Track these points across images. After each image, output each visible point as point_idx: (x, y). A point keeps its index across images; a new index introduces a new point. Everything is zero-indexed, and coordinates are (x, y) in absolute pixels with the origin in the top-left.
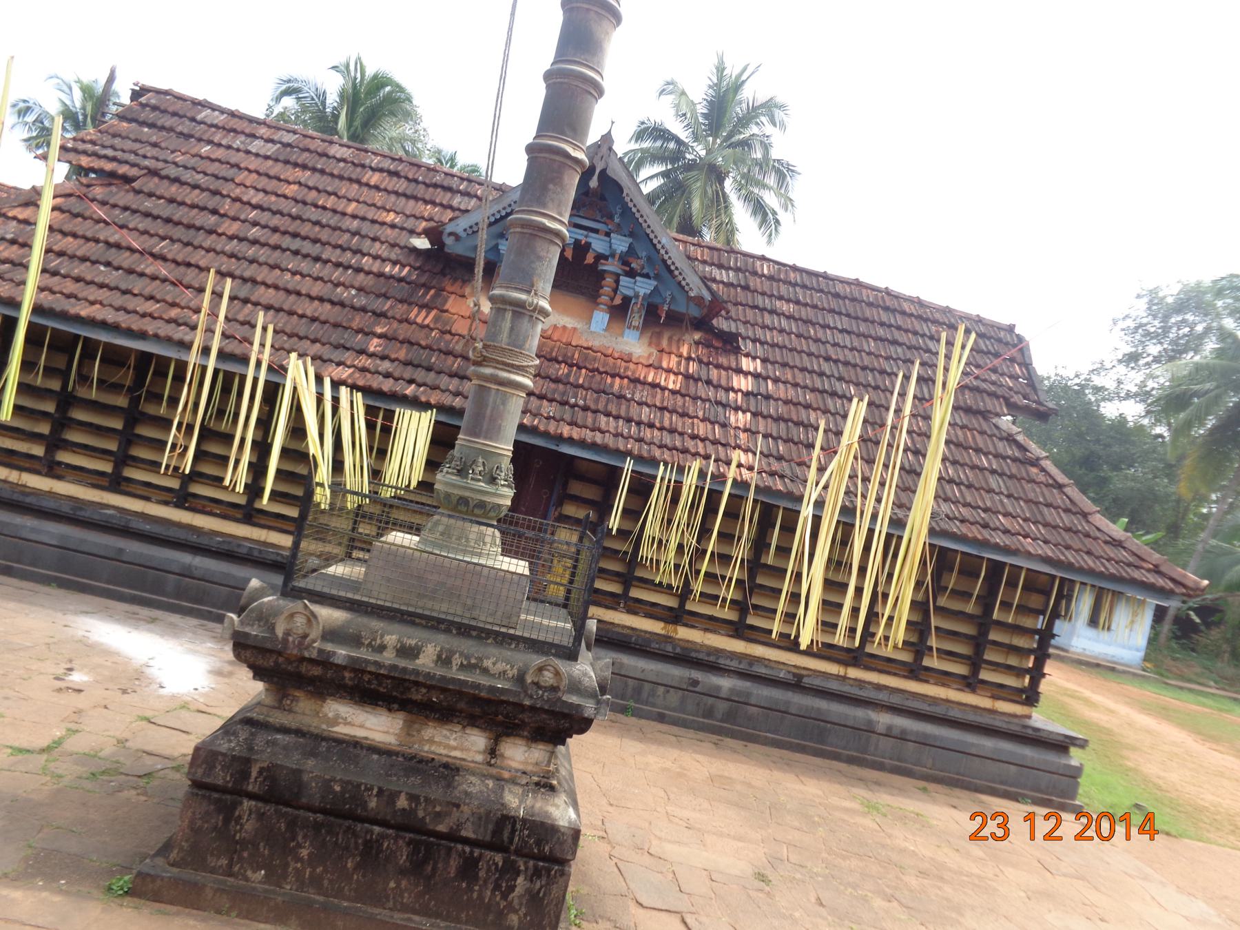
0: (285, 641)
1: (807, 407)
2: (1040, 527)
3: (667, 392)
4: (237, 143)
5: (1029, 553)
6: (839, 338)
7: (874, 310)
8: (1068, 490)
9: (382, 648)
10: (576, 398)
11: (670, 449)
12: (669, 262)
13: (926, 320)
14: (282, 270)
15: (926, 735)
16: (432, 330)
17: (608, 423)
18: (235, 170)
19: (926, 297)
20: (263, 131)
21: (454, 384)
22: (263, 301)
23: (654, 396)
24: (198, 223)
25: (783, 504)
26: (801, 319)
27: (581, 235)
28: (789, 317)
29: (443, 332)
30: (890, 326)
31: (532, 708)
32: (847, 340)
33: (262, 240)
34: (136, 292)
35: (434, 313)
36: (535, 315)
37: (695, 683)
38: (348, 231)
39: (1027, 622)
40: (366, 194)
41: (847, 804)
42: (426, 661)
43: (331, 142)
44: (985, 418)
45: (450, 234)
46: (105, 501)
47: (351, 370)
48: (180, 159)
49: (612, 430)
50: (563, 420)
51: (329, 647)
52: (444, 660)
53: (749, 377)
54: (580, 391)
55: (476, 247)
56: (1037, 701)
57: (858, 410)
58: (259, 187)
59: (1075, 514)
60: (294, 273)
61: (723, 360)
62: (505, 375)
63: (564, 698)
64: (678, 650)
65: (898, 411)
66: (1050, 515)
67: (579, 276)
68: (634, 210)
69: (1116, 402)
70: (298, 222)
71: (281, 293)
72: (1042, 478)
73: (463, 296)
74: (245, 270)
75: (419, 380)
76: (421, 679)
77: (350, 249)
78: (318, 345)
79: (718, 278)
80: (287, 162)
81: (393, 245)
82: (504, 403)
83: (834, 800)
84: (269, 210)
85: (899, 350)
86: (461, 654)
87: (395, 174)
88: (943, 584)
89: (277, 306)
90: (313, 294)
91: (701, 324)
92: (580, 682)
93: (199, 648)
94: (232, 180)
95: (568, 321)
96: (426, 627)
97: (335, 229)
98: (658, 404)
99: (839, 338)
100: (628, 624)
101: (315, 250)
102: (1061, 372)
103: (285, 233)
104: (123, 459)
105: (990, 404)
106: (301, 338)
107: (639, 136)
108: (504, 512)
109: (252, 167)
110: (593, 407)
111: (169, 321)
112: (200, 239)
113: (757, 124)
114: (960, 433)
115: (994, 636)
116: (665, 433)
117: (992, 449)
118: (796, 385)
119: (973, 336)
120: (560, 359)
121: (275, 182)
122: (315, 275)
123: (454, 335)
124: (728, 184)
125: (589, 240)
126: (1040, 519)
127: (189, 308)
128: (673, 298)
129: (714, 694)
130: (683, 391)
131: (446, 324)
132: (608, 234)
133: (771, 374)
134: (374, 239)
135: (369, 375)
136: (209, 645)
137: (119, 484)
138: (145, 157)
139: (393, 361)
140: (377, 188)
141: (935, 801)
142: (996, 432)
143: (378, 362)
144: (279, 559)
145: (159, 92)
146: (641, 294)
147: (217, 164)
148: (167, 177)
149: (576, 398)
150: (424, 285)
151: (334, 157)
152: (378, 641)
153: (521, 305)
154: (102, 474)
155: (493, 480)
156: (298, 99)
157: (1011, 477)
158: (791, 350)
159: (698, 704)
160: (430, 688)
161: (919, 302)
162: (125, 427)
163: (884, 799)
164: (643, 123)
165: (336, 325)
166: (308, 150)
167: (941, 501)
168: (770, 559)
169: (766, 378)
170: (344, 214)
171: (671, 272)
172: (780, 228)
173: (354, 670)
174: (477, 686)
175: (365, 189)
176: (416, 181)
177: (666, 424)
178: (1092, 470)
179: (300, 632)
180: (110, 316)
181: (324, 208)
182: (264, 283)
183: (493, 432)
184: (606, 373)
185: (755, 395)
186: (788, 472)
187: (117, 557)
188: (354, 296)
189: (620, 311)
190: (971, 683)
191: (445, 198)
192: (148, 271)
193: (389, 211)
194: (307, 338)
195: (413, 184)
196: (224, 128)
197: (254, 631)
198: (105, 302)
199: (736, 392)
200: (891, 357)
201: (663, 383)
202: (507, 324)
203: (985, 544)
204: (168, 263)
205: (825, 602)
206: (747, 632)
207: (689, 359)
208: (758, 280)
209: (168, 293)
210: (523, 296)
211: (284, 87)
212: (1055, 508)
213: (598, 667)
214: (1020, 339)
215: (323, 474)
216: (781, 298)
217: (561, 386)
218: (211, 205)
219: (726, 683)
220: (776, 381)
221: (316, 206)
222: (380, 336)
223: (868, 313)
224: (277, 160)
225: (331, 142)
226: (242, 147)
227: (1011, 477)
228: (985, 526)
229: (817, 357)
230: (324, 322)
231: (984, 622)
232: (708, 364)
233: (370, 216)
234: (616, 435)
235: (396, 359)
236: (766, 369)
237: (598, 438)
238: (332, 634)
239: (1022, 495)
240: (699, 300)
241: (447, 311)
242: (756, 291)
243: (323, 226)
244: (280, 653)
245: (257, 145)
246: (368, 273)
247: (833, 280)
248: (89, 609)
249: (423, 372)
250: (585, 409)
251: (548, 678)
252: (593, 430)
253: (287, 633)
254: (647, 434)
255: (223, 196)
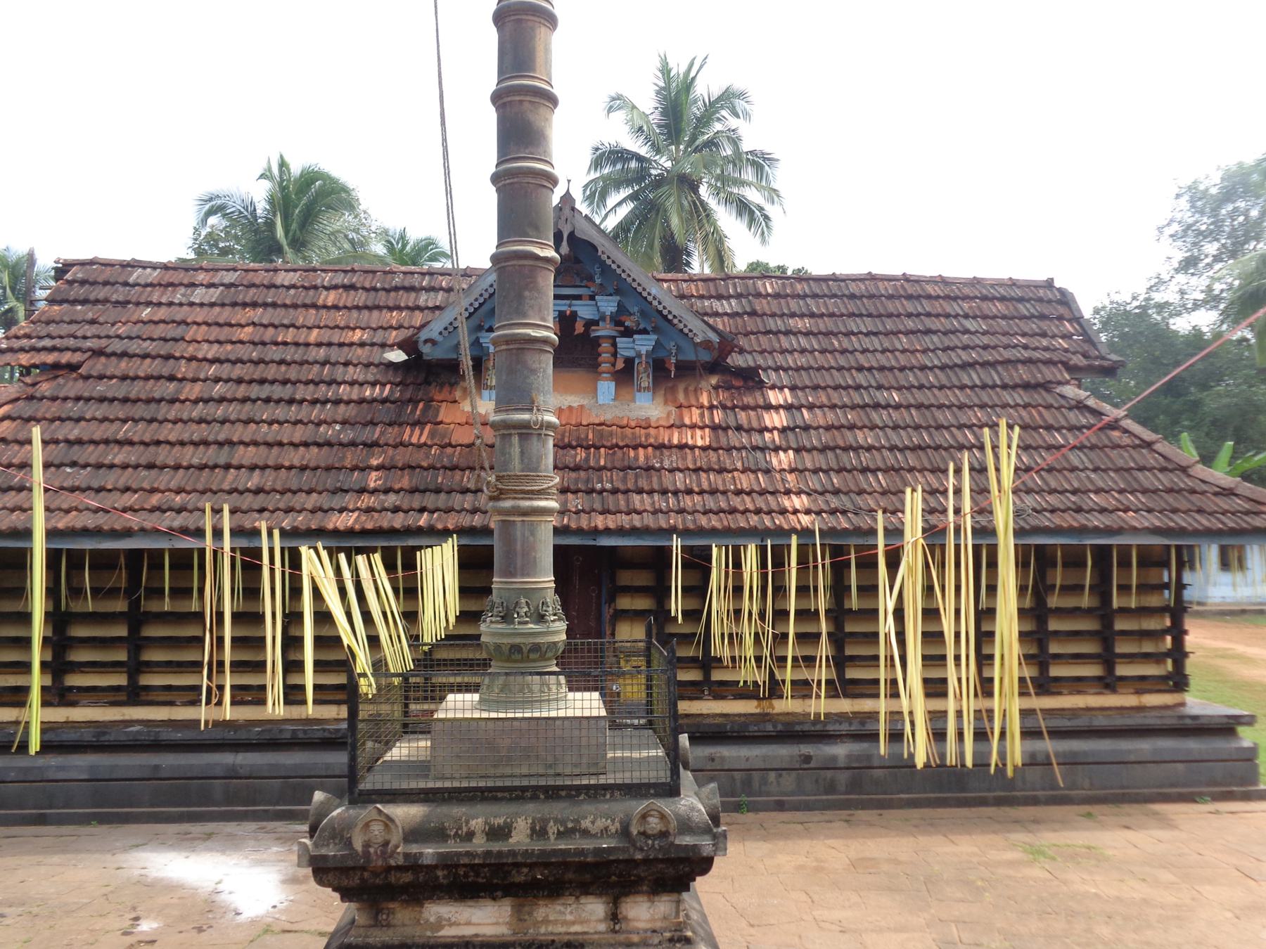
0: (366, 854)
1: (852, 427)
2: (1139, 495)
3: (697, 451)
4: (178, 298)
5: (1135, 529)
6: (867, 342)
7: (897, 302)
8: (1158, 447)
9: (470, 835)
10: (602, 482)
11: (716, 513)
12: (665, 312)
13: (955, 299)
14: (257, 423)
15: (1074, 754)
16: (431, 447)
17: (642, 501)
18: (183, 327)
19: (949, 273)
20: (201, 277)
21: (468, 501)
22: (246, 462)
23: (684, 459)
24: (157, 395)
25: (853, 541)
26: (820, 333)
27: (564, 306)
28: (807, 334)
29: (443, 447)
30: (918, 315)
31: (646, 861)
32: (875, 343)
33: (228, 396)
34: (109, 487)
35: (428, 427)
36: (544, 432)
37: (807, 759)
38: (316, 362)
39: (1153, 601)
40: (326, 317)
41: (1009, 855)
42: (520, 838)
43: (276, 270)
44: (1048, 390)
45: (426, 341)
46: (127, 718)
47: (356, 514)
48: (122, 330)
49: (649, 508)
50: (594, 510)
51: (414, 849)
52: (539, 832)
53: (782, 411)
54: (604, 472)
55: (458, 345)
56: (1187, 684)
57: (914, 502)
58: (211, 339)
59: (1171, 471)
60: (270, 423)
61: (748, 400)
62: (527, 503)
63: (677, 842)
64: (780, 727)
65: (957, 511)
66: (1146, 479)
67: (576, 350)
68: (614, 266)
69: (1185, 315)
70: (262, 365)
71: (262, 448)
72: (1126, 440)
73: (455, 401)
74: (218, 433)
75: (430, 506)
76: (520, 859)
77: (323, 382)
78: (314, 495)
79: (720, 311)
80: (234, 304)
81: (368, 365)
82: (533, 534)
83: (994, 855)
84: (228, 361)
85: (935, 338)
86: (556, 821)
87: (352, 287)
88: (1049, 582)
89: (261, 464)
90: (296, 440)
91: (715, 367)
92: (689, 819)
93: (265, 856)
94: (183, 339)
95: (573, 400)
96: (511, 799)
97: (301, 363)
98: (691, 466)
99: (867, 342)
100: (718, 711)
101: (286, 392)
102: (1116, 298)
103: (251, 382)
104: (136, 667)
105: (1049, 373)
106: (294, 493)
107: (597, 163)
108: (561, 648)
109: (199, 320)
110: (622, 487)
111: (152, 510)
112: (163, 411)
113: (719, 119)
114: (1024, 413)
115: (1119, 625)
116: (706, 496)
117: (1064, 423)
118: (833, 407)
119: (1017, 429)
120: (574, 443)
121: (227, 329)
122: (293, 420)
123: (455, 447)
124: (703, 191)
125: (574, 308)
126: (1136, 486)
127: (170, 490)
128: (679, 348)
129: (830, 765)
130: (714, 445)
131: (443, 436)
132: (592, 298)
133: (804, 402)
134: (346, 364)
135: (376, 515)
136: (275, 849)
137: (138, 695)
138: (85, 338)
139: (397, 492)
140: (335, 307)
141: (1103, 826)
142: (1063, 402)
143: (382, 497)
144: (327, 735)
145: (83, 264)
146: (644, 352)
147: (162, 326)
148: (114, 354)
149: (602, 482)
150: (410, 400)
151: (283, 286)
152: (465, 829)
153: (525, 425)
154: (117, 689)
155: (541, 618)
156: (224, 216)
157: (1093, 447)
158: (818, 369)
159: (817, 781)
160: (532, 866)
161: (943, 281)
162: (130, 631)
163: (1048, 838)
164: (597, 149)
165: (328, 469)
166: (253, 285)
167: (1022, 495)
168: (854, 602)
169: (799, 408)
170: (307, 345)
171: (670, 321)
172: (771, 224)
173: (446, 867)
174: (581, 852)
175: (324, 312)
176: (375, 289)
177: (705, 486)
178: (1179, 395)
179: (380, 840)
180: (89, 521)
181: (285, 344)
182: (241, 443)
183: (529, 567)
184: (627, 446)
185: (792, 429)
186: (849, 506)
187: (154, 776)
188: (339, 432)
189: (625, 375)
190: (1109, 683)
191: (410, 299)
192: (116, 461)
193: (354, 329)
194: (300, 490)
195: (373, 293)
196: (160, 285)
197: (330, 851)
198: (80, 507)
199: (770, 431)
200: (929, 349)
201: (690, 442)
202: (516, 450)
203: (1083, 530)
204: (137, 447)
205: (926, 681)
206: (851, 688)
207: (711, 407)
208: (764, 301)
209: (144, 478)
210: (526, 416)
211: (207, 207)
212: (1150, 470)
213: (703, 796)
214: (1062, 292)
215: (363, 662)
216: (793, 315)
217: (582, 474)
218: (166, 372)
219: (841, 751)
220: (811, 407)
221: (276, 344)
222: (377, 468)
223: (891, 306)
224: (223, 305)
225: (276, 270)
226: (184, 300)
227: (1093, 447)
228: (1079, 510)
229: (849, 369)
230: (316, 469)
231: (1105, 613)
232: (733, 408)
233: (335, 340)
234: (655, 512)
235: (401, 489)
236: (796, 397)
237: (637, 521)
238: (413, 834)
239: (1111, 466)
240: (707, 344)
241: (441, 422)
242: (765, 314)
243: (289, 364)
244: (363, 869)
245: (199, 295)
246: (348, 402)
247: (843, 280)
248: (139, 841)
249: (433, 496)
250: (615, 491)
251: (654, 824)
252: (628, 513)
253: (367, 845)
254: (687, 502)
255: (177, 359)
